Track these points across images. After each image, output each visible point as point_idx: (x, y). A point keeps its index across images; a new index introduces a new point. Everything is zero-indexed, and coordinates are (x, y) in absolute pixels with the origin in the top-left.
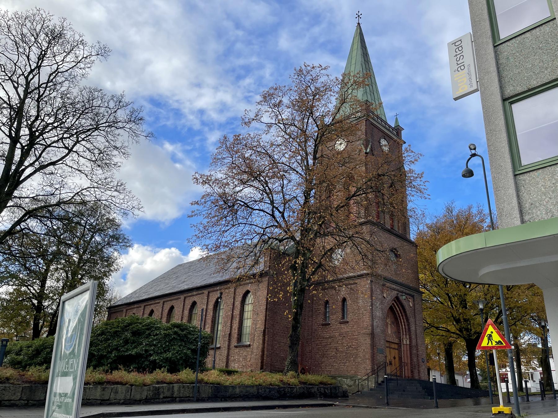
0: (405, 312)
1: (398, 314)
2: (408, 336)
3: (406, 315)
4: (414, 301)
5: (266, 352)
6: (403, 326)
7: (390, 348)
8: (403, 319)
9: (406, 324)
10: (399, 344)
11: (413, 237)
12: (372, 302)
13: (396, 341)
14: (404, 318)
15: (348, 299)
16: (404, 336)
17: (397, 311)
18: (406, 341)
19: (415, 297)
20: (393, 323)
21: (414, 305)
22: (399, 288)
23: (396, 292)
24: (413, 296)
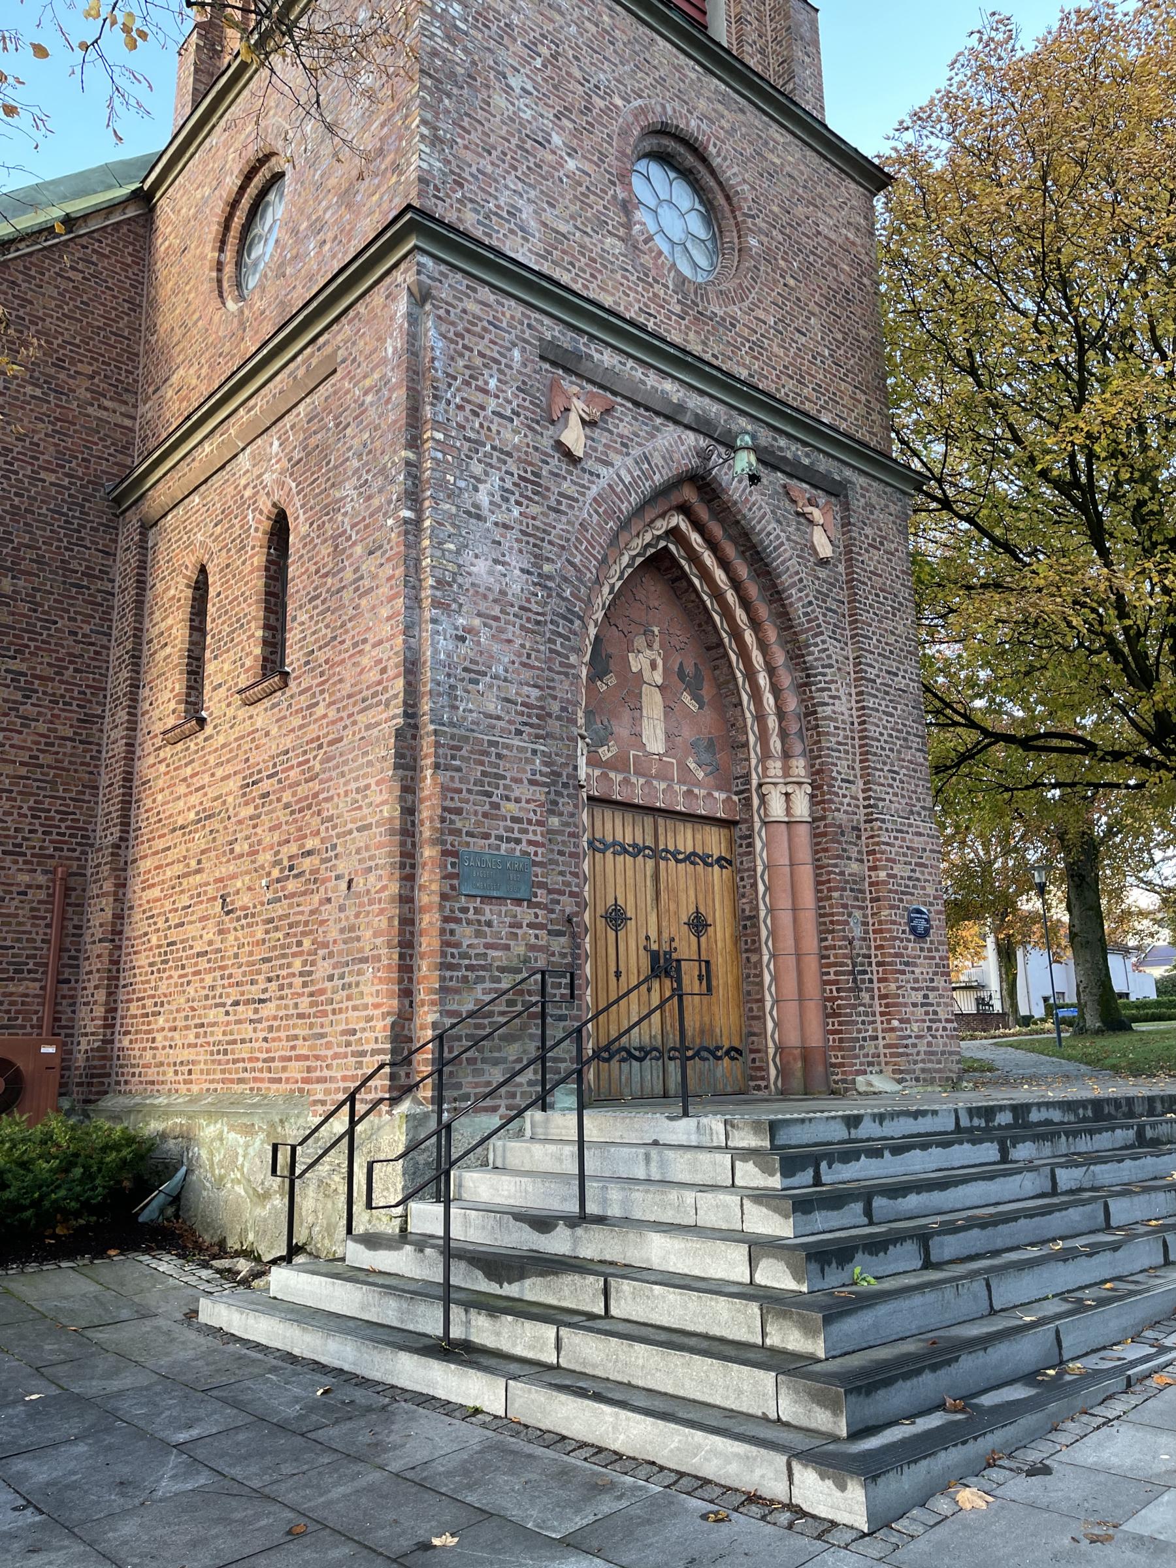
0: (776, 595)
1: (727, 613)
2: (799, 767)
3: (784, 618)
4: (846, 524)
6: (765, 700)
7: (657, 854)
8: (763, 646)
9: (785, 680)
12: (413, 469)
13: (717, 803)
14: (772, 635)
17: (718, 596)
18: (785, 800)
19: (858, 503)
20: (680, 679)
21: (848, 553)
22: (714, 409)
23: (690, 438)
24: (836, 490)
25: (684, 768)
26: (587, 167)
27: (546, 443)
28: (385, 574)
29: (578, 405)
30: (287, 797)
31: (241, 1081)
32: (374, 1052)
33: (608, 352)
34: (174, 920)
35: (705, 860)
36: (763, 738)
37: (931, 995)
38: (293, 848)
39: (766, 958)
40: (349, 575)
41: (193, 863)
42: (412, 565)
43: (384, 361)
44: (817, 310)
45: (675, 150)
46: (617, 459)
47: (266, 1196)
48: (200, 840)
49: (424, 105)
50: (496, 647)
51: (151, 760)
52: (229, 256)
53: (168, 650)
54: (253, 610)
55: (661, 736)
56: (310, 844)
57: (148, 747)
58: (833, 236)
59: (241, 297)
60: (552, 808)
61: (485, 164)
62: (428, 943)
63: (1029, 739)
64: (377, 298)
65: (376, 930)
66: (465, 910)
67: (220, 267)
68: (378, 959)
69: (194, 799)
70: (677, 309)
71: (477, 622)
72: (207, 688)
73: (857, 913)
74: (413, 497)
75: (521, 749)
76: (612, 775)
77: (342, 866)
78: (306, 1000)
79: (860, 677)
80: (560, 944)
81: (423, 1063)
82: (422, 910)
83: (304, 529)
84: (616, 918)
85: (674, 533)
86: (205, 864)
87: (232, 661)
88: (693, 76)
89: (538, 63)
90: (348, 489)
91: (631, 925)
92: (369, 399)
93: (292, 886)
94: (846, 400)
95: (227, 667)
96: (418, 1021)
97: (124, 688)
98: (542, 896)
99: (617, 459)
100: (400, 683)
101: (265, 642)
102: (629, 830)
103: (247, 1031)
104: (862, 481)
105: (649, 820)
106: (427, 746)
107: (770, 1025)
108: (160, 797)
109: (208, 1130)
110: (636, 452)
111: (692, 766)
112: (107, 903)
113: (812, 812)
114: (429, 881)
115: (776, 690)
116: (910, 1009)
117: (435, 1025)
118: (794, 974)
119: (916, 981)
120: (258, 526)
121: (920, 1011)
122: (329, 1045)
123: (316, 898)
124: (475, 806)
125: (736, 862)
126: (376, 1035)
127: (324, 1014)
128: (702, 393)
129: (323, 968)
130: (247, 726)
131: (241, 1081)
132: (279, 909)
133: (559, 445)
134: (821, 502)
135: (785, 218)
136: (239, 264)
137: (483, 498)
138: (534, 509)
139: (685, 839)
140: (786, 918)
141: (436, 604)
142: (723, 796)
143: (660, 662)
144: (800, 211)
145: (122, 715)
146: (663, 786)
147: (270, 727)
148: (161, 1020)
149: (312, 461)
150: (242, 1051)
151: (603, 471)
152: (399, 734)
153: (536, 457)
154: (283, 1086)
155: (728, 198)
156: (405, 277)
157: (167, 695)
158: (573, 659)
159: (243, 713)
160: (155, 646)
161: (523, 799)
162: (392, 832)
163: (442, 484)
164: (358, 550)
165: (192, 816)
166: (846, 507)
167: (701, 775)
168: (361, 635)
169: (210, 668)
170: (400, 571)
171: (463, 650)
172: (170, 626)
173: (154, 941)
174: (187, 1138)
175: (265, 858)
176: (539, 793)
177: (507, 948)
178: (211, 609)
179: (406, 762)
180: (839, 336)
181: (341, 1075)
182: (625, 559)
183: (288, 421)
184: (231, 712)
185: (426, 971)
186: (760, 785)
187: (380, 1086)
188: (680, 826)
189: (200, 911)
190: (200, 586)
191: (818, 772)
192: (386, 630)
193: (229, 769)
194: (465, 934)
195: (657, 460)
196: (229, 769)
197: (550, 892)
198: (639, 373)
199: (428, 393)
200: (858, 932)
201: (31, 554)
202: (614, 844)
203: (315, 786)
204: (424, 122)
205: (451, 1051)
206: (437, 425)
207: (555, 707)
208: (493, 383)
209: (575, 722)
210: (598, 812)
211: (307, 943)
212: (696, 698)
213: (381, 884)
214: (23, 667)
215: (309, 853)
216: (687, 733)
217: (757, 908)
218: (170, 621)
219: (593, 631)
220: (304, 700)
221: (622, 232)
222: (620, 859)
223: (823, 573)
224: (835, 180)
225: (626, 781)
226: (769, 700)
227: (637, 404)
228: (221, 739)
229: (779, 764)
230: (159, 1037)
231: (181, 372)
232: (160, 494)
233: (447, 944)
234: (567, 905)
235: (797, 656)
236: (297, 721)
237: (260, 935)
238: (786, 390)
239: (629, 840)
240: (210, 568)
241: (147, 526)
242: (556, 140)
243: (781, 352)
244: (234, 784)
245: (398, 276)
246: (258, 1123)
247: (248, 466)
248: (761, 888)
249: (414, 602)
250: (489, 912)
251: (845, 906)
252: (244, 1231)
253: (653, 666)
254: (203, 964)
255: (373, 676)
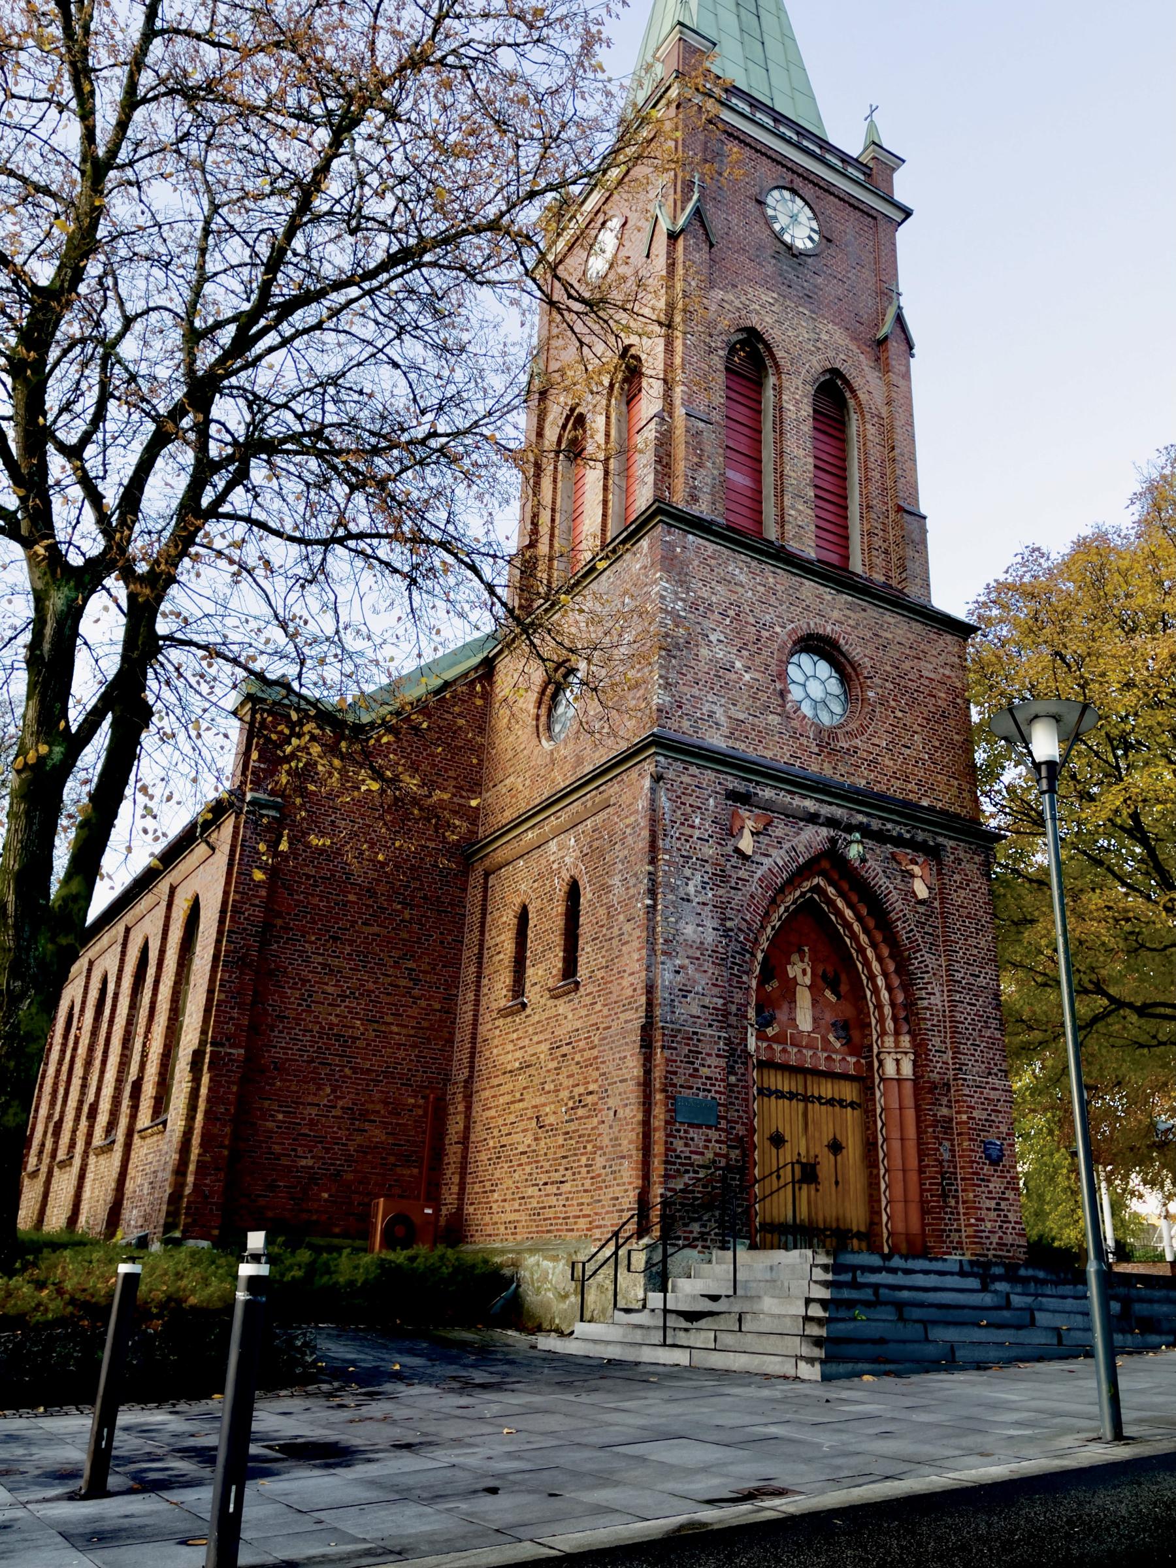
1: (854, 937)
2: (905, 1041)
3: (892, 939)
5: (195, 1151)
7: (806, 1099)
10: (865, 1080)
11: (953, 590)
15: (583, 882)
16: (889, 1041)
18: (896, 1064)
23: (824, 832)
24: (934, 853)
25: (825, 1040)
26: (757, 675)
27: (729, 849)
28: (635, 935)
29: (749, 824)
30: (578, 1058)
31: (549, 1231)
32: (629, 1210)
33: (767, 790)
34: (505, 1130)
35: (841, 1103)
36: (881, 1020)
37: (1003, 1203)
38: (581, 1089)
39: (882, 1172)
40: (616, 931)
41: (518, 1095)
42: (651, 930)
43: (637, 811)
44: (919, 729)
45: (817, 645)
46: (774, 852)
47: (566, 1296)
48: (522, 1080)
49: (662, 666)
50: (697, 976)
51: (489, 1026)
52: (543, 711)
53: (501, 956)
54: (557, 939)
55: (809, 1019)
56: (592, 1087)
57: (487, 1017)
58: (932, 676)
59: (551, 738)
60: (731, 1070)
61: (697, 693)
62: (658, 1149)
63: (1145, 1006)
64: (634, 773)
65: (629, 1141)
66: (678, 1131)
67: (538, 717)
68: (631, 1156)
69: (519, 1054)
70: (816, 750)
71: (687, 961)
72: (528, 985)
73: (947, 1144)
74: (652, 893)
75: (712, 1036)
76: (775, 1046)
77: (611, 1102)
78: (589, 1181)
79: (952, 981)
80: (735, 1154)
81: (655, 1215)
82: (655, 1130)
83: (589, 896)
84: (778, 1140)
85: (817, 889)
86: (526, 1096)
87: (544, 970)
88: (829, 597)
89: (728, 621)
90: (616, 880)
91: (788, 1145)
92: (628, 831)
93: (581, 1112)
94: (942, 787)
95: (540, 972)
96: (652, 1194)
97: (473, 977)
98: (723, 1124)
99: (774, 852)
100: (643, 999)
101: (565, 959)
102: (786, 1082)
103: (553, 1200)
104: (952, 843)
105: (800, 1078)
106: (658, 1035)
107: (885, 1218)
108: (495, 1051)
109: (531, 1260)
110: (787, 846)
111: (832, 1039)
112: (460, 1118)
113: (914, 1074)
114: (659, 1114)
115: (889, 988)
116: (984, 1212)
117: (662, 1195)
118: (901, 1184)
119: (990, 1192)
120: (560, 888)
121: (993, 1215)
122: (603, 1207)
123: (595, 1120)
124: (684, 1072)
125: (865, 1105)
126: (629, 1199)
127: (600, 1188)
128: (830, 804)
129: (600, 1161)
130: (553, 1012)
131: (549, 1231)
132: (572, 1127)
133: (737, 850)
134: (920, 860)
135: (897, 672)
136: (549, 715)
137: (691, 889)
138: (721, 892)
139: (827, 1089)
140: (896, 1145)
141: (664, 953)
142: (854, 1060)
143: (809, 970)
144: (907, 665)
145: (471, 996)
146: (811, 1053)
147: (569, 1015)
148: (496, 1195)
149: (593, 854)
150: (549, 1213)
151: (765, 860)
152: (643, 1028)
153: (722, 860)
154: (575, 1234)
155: (855, 669)
156: (649, 767)
157: (500, 985)
158: (745, 978)
159: (551, 1003)
160: (492, 951)
161: (712, 1066)
162: (639, 1084)
163: (668, 884)
164: (621, 917)
165: (517, 1065)
166: (940, 863)
167: (838, 1045)
168: (619, 963)
169: (530, 972)
170: (644, 934)
171: (679, 978)
172: (503, 941)
173: (491, 1144)
174: (515, 1264)
175: (564, 1094)
176: (722, 1062)
177: (702, 1154)
178: (530, 935)
179: (647, 1043)
180: (937, 744)
181: (611, 1222)
182: (798, 893)
183: (580, 828)
184: (543, 1001)
185: (657, 1164)
186: (879, 1053)
187: (632, 1227)
188: (823, 1081)
189: (522, 1125)
190: (523, 917)
191: (919, 1045)
192: (637, 967)
193: (541, 1037)
194: (679, 1145)
195: (801, 848)
196: (541, 1037)
197: (729, 1122)
198: (788, 799)
199: (660, 833)
200: (947, 1156)
201: (420, 894)
202: (777, 1091)
203: (595, 1052)
204: (661, 677)
205: (230, 211)
206: (666, 851)
207: (733, 1008)
208: (697, 821)
209: (746, 1017)
210: (765, 1072)
211: (589, 1147)
212: (835, 992)
213: (632, 1113)
214: (414, 966)
215: (591, 1093)
216: (829, 1017)
217: (876, 1138)
218: (503, 937)
219: (760, 956)
220: (588, 1000)
221: (779, 710)
222: (780, 1101)
223: (921, 909)
224: (935, 637)
225: (784, 1051)
226: (885, 995)
227: (787, 816)
228: (536, 1018)
229: (892, 1039)
230: (494, 1206)
231: (512, 779)
232: (501, 855)
233: (667, 1149)
234: (740, 1130)
235: (903, 967)
236: (584, 1012)
237: (561, 1142)
238: (895, 788)
239: (786, 1089)
240: (530, 908)
241: (487, 875)
242: (738, 665)
243: (891, 763)
244: (545, 1047)
245: (645, 765)
246: (561, 1254)
247: (555, 849)
248: (879, 1124)
249: (652, 952)
250: (692, 1133)
251: (937, 1138)
252: (553, 1318)
253: (804, 972)
254: (524, 1159)
255: (629, 992)
